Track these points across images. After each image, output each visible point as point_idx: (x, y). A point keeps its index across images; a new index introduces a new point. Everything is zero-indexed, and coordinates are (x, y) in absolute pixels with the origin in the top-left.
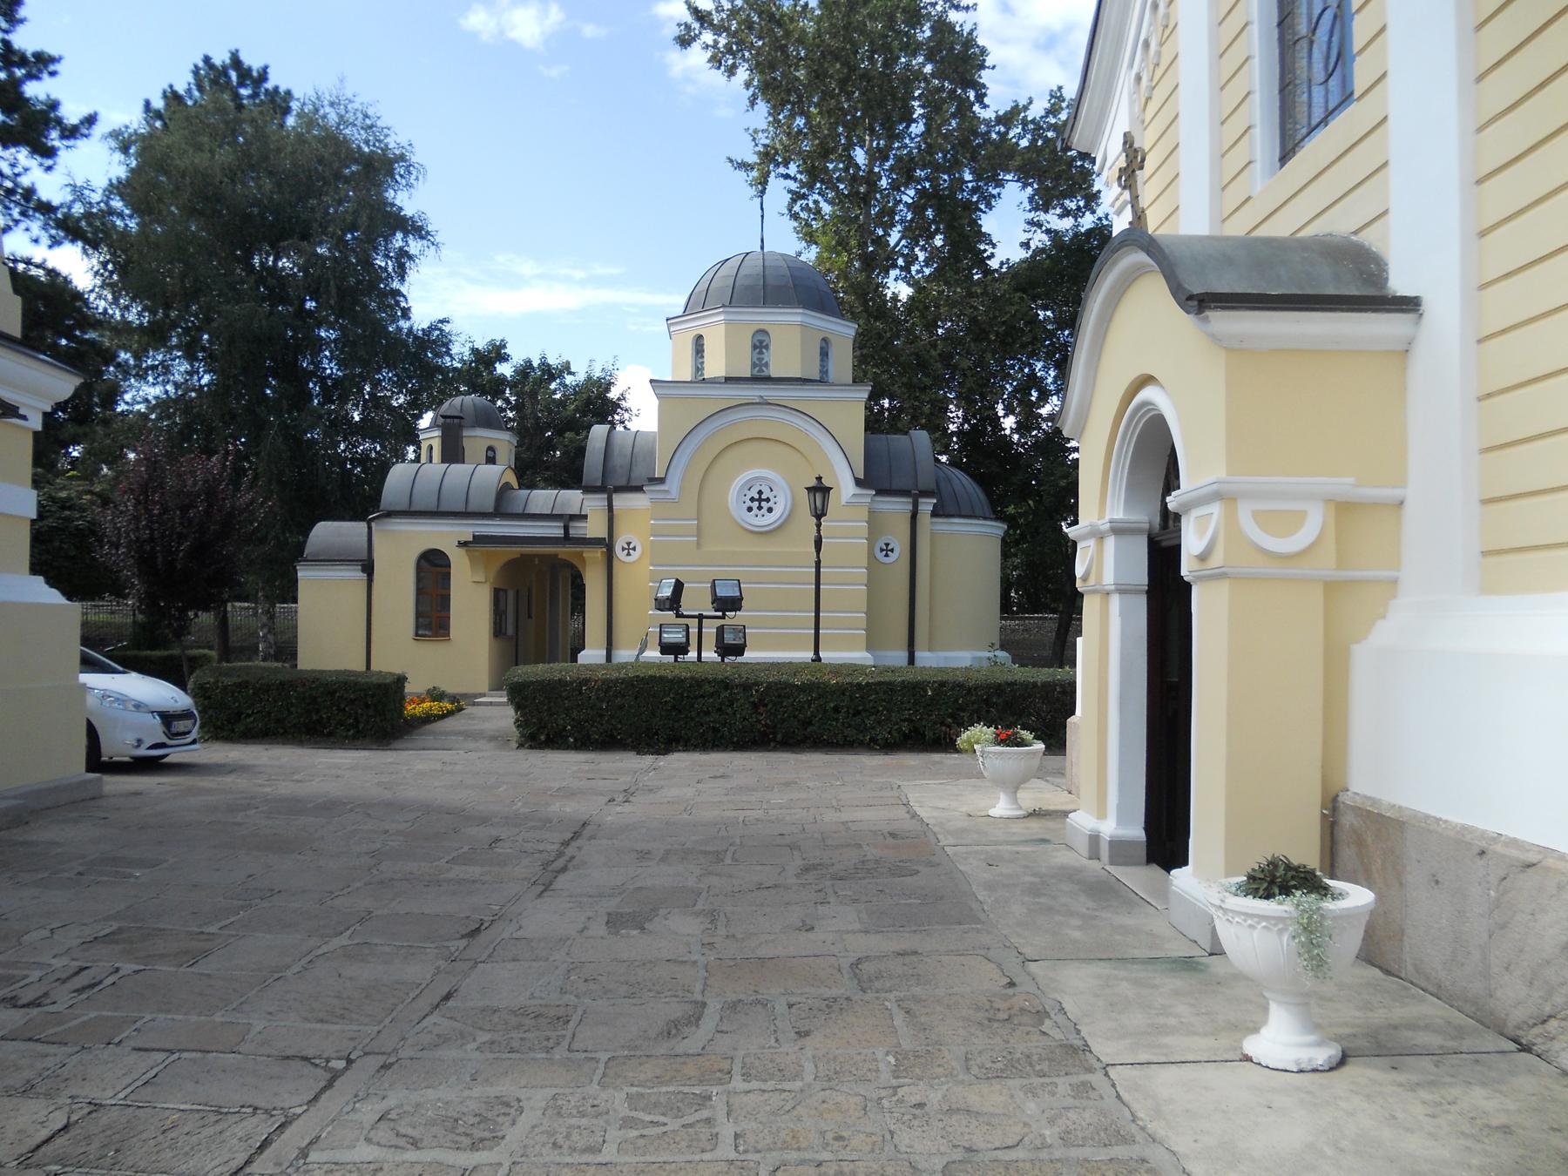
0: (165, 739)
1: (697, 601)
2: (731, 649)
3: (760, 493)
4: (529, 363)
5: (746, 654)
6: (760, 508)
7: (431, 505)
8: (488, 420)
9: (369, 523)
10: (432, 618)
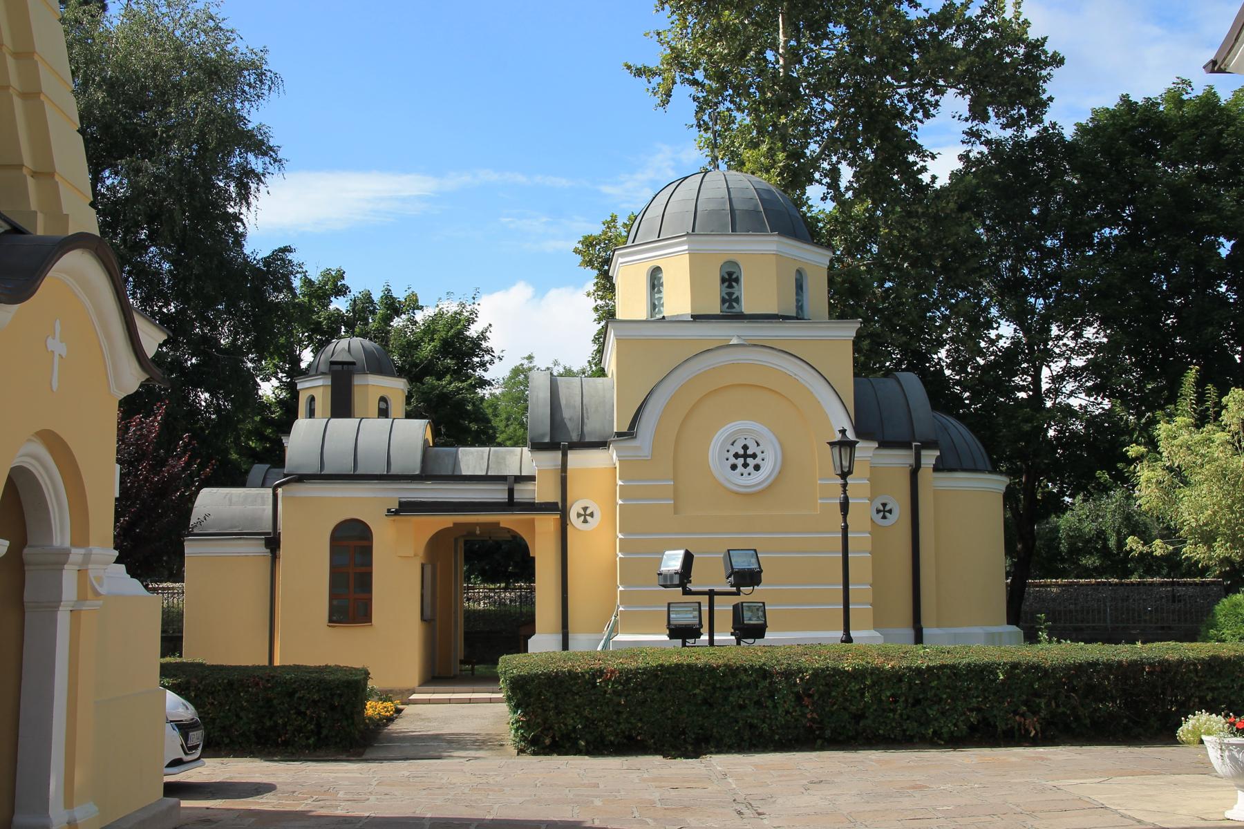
0: (181, 755)
2: (748, 630)
3: (745, 447)
4: (368, 298)
6: (745, 465)
7: (347, 467)
8: (378, 366)
9: (275, 488)
10: (351, 599)
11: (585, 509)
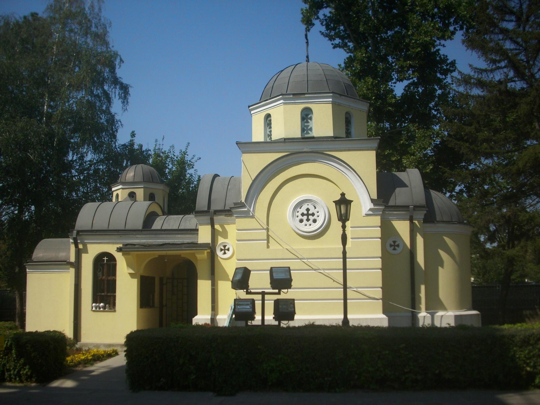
1: (260, 281)
3: (308, 210)
5: (296, 317)
6: (308, 220)
11: (391, 246)
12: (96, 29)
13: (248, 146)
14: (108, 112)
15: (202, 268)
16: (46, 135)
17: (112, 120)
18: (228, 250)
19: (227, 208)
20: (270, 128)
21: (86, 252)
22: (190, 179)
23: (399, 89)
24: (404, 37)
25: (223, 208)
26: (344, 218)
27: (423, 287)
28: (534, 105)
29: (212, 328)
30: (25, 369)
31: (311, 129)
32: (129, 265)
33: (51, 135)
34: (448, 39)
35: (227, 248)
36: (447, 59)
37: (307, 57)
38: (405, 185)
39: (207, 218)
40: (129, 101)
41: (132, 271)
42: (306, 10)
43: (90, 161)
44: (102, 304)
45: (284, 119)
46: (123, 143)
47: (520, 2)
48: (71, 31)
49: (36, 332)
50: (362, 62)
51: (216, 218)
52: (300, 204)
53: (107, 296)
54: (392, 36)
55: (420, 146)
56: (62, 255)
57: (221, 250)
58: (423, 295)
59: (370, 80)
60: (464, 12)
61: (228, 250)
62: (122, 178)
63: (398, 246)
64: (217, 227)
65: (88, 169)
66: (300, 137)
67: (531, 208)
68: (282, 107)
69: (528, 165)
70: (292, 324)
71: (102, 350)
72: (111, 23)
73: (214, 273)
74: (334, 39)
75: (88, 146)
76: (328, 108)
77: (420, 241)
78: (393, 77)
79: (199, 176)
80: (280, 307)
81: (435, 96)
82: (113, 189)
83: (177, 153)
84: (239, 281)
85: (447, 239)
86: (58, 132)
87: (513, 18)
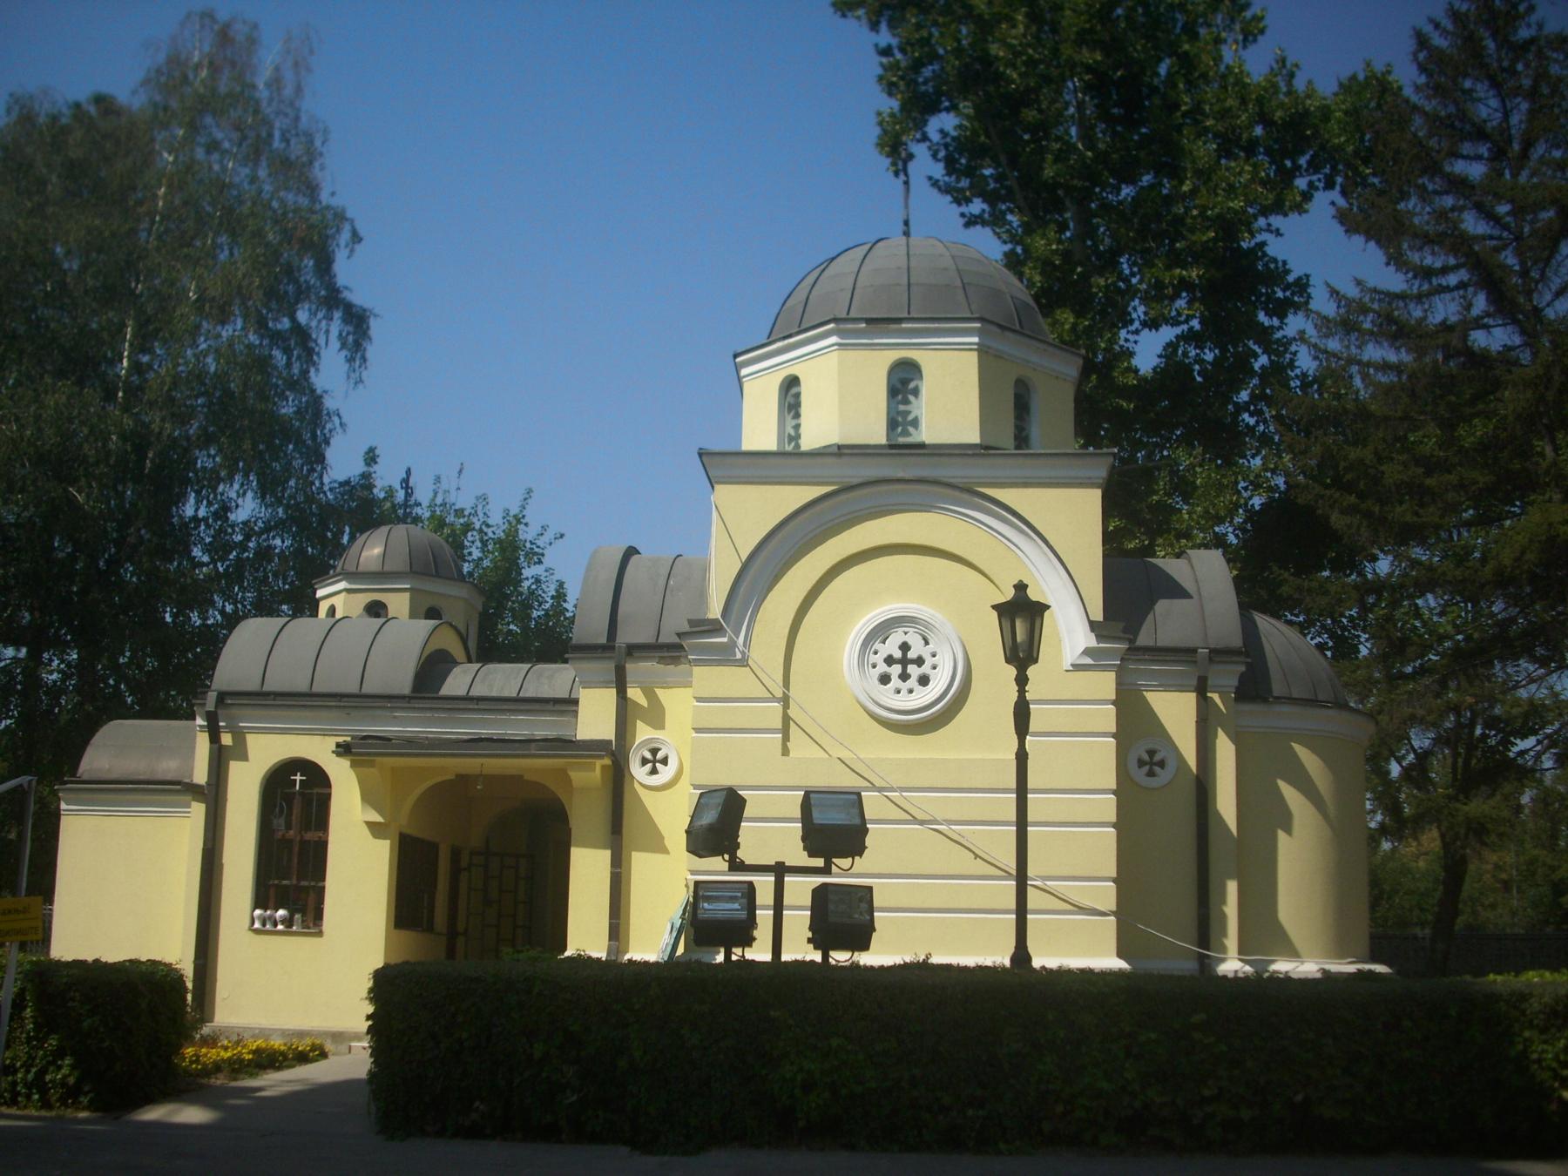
1: (771, 835)
3: (905, 647)
6: (904, 677)
11: (1141, 763)
12: (283, 145)
13: (726, 464)
14: (300, 384)
15: (585, 813)
16: (124, 437)
17: (314, 411)
18: (665, 761)
19: (668, 637)
20: (797, 416)
21: (244, 757)
22: (532, 593)
23: (1147, 351)
24: (1168, 201)
25: (652, 640)
26: (1022, 655)
27: (1232, 887)
28: (1547, 388)
29: (618, 983)
30: (59, 1068)
31: (915, 423)
32: (368, 798)
33: (139, 441)
34: (1291, 209)
35: (660, 755)
36: (1287, 272)
37: (906, 223)
38: (1184, 594)
39: (607, 667)
40: (369, 355)
41: (376, 818)
42: (892, 115)
43: (245, 523)
44: (281, 912)
45: (838, 393)
46: (342, 478)
47: (1504, 106)
48: (213, 146)
49: (97, 961)
50: (1046, 266)
51: (631, 667)
52: (881, 631)
53: (299, 889)
54: (1137, 201)
55: (1207, 512)
56: (168, 767)
57: (644, 761)
58: (1231, 909)
59: (1067, 317)
60: (1339, 136)
61: (665, 761)
62: (347, 562)
63: (1162, 764)
64: (634, 693)
65: (243, 546)
66: (883, 441)
67: (1533, 687)
68: (834, 357)
69: (1529, 556)
70: (866, 959)
71: (277, 1043)
72: (326, 131)
73: (620, 827)
74: (968, 201)
75: (246, 476)
76: (968, 364)
77: (1225, 751)
78: (1134, 316)
79: (561, 584)
80: (832, 907)
81: (1252, 373)
82: (320, 593)
83: (496, 518)
84: (711, 828)
85: (1301, 751)
86: (162, 429)
87: (1484, 150)
